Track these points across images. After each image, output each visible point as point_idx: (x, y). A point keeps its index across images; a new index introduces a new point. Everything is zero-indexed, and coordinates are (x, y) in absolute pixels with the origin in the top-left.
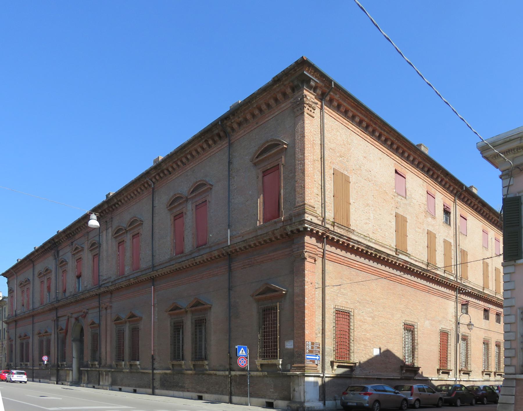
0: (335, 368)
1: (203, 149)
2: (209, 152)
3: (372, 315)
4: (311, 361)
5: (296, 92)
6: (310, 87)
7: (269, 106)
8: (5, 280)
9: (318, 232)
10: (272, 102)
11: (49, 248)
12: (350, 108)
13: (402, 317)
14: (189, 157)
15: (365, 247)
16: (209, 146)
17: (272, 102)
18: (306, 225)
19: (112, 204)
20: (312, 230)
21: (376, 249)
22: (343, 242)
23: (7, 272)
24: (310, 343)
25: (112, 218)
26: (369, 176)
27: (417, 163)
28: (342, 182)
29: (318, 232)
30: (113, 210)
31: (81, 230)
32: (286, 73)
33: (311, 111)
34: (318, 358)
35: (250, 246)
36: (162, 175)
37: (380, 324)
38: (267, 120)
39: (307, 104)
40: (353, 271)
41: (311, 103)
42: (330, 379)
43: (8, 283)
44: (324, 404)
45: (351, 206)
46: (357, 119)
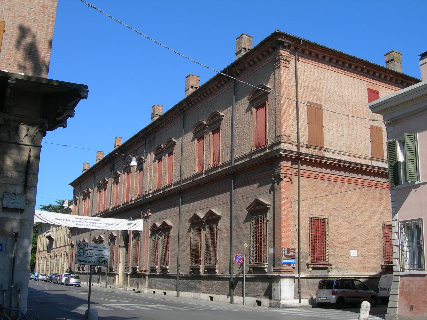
0: (310, 269)
1: (218, 87)
2: (222, 90)
3: (348, 219)
4: (287, 264)
5: (275, 51)
6: (284, 48)
7: (259, 59)
8: (72, 188)
9: (291, 156)
10: (261, 57)
11: (107, 161)
12: (319, 53)
13: (381, 218)
14: (208, 92)
15: (338, 162)
16: (222, 85)
17: (261, 57)
18: (281, 153)
19: (155, 126)
20: (286, 156)
21: (348, 162)
22: (316, 161)
23: (74, 182)
24: (286, 249)
25: (154, 138)
26: (342, 100)
27: (389, 79)
28: (316, 112)
29: (291, 156)
30: (156, 131)
31: (132, 147)
32: (267, 40)
33: (286, 63)
34: (293, 261)
35: (246, 167)
36: (190, 105)
37: (357, 227)
38: (258, 68)
39: (283, 60)
40: (328, 184)
41: (285, 58)
42: (365, 279)
43: (74, 191)
44: (300, 302)
45: (324, 129)
46: (327, 59)
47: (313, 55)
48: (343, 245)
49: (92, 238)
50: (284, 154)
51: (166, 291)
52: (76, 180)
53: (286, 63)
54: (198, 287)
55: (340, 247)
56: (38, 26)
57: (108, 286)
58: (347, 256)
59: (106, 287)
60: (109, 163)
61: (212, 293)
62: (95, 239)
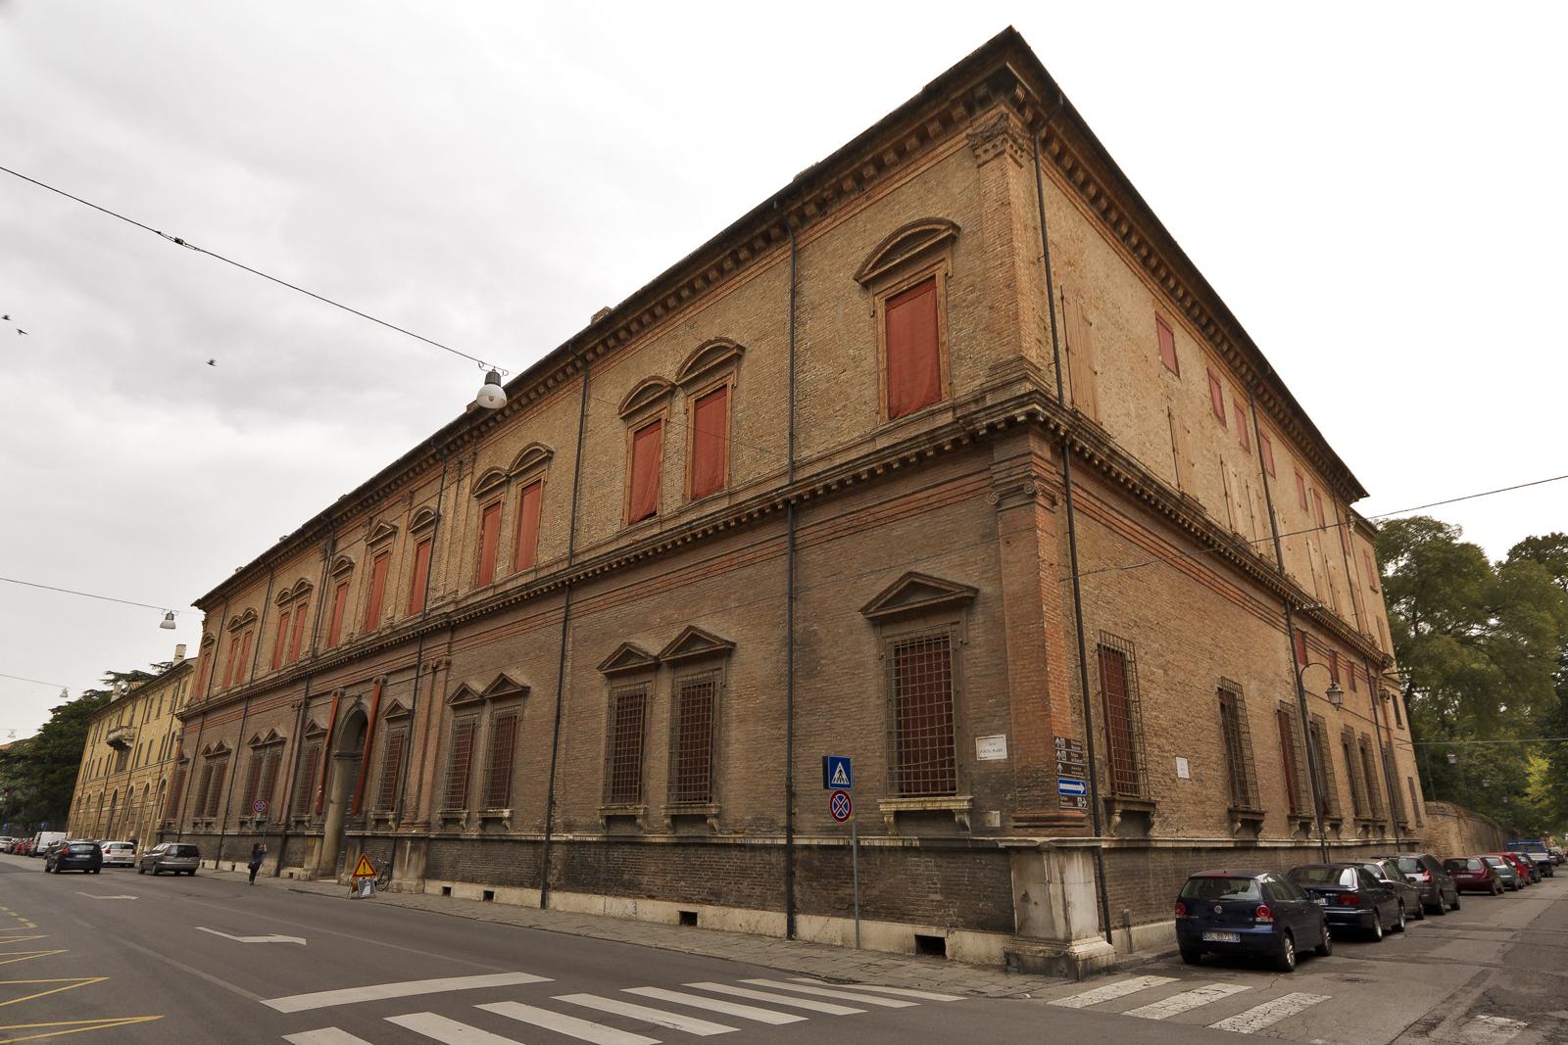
25: (475, 454)
38: (896, 186)
49: (203, 747)
51: (497, 890)
52: (258, 559)
54: (626, 877)
57: (285, 872)
59: (277, 874)
60: (322, 537)
61: (687, 900)
62: (208, 750)
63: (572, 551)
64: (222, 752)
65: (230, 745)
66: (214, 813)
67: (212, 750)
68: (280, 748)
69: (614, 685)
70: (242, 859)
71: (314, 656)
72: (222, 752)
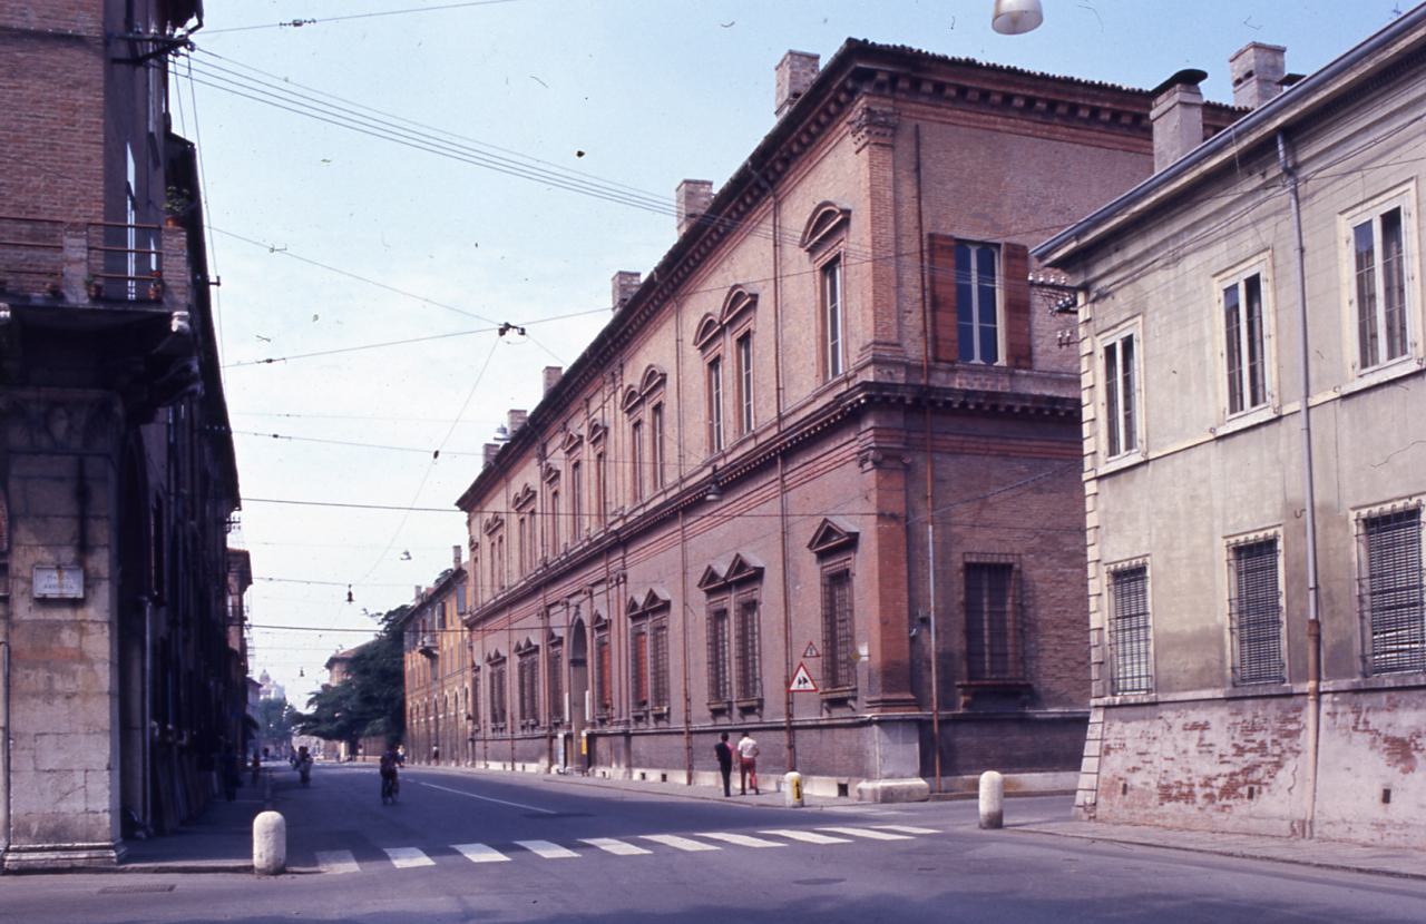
47: (970, 95)
48: (1067, 631)
50: (894, 397)
53: (884, 135)
55: (1059, 636)
56: (63, 161)
58: (1081, 659)
63: (779, 414)
64: (656, 606)
65: (504, 653)
66: (503, 720)
67: (523, 646)
68: (535, 656)
69: (825, 564)
70: (675, 766)
71: (546, 565)
72: (745, 576)
